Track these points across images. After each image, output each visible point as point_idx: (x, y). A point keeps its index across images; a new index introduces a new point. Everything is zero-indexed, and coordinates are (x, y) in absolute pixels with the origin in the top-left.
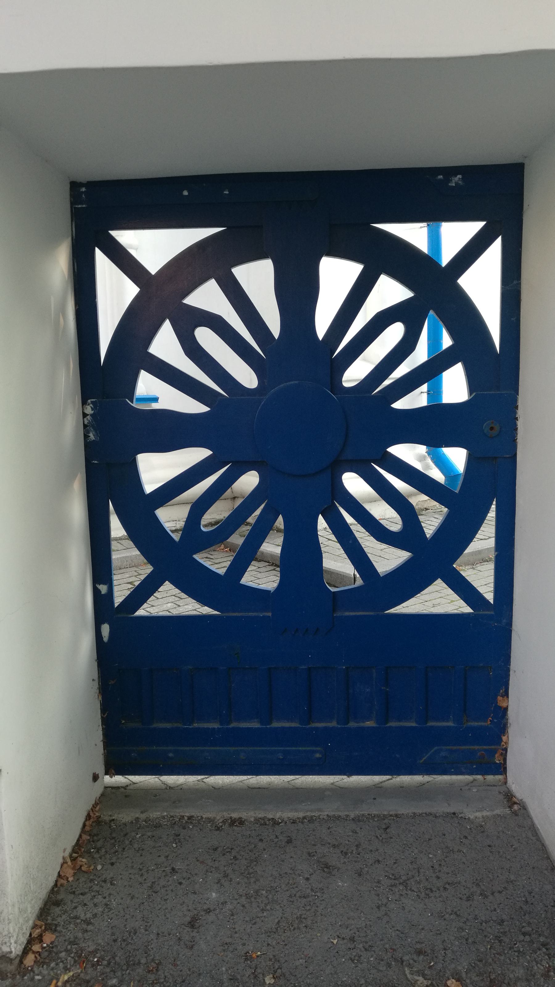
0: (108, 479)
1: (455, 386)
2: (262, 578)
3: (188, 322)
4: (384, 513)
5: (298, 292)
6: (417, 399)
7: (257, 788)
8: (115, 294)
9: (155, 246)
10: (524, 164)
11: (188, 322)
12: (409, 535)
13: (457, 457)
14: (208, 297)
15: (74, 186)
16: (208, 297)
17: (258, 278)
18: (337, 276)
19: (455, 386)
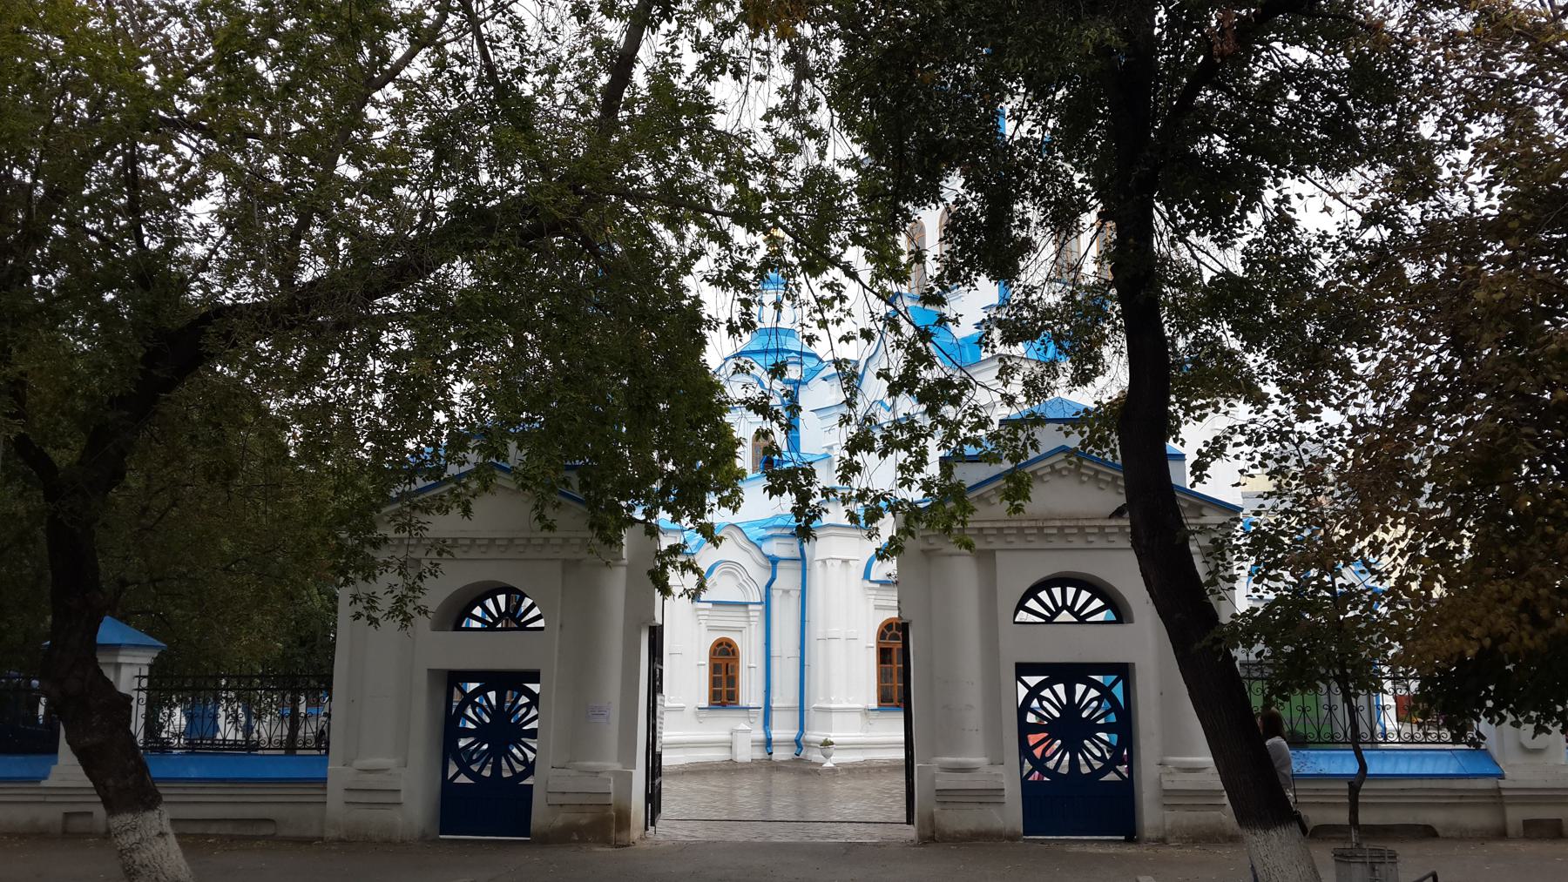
0: (449, 749)
1: (1112, 718)
2: (487, 773)
3: (1041, 699)
4: (519, 755)
5: (1070, 692)
6: (1102, 721)
7: (1452, 838)
8: (457, 698)
9: (1033, 681)
10: (430, 671)
11: (1041, 699)
12: (1044, 759)
13: (1115, 737)
14: (1046, 693)
15: (430, 671)
16: (1046, 693)
17: (1060, 688)
18: (1080, 688)
19: (1112, 718)
